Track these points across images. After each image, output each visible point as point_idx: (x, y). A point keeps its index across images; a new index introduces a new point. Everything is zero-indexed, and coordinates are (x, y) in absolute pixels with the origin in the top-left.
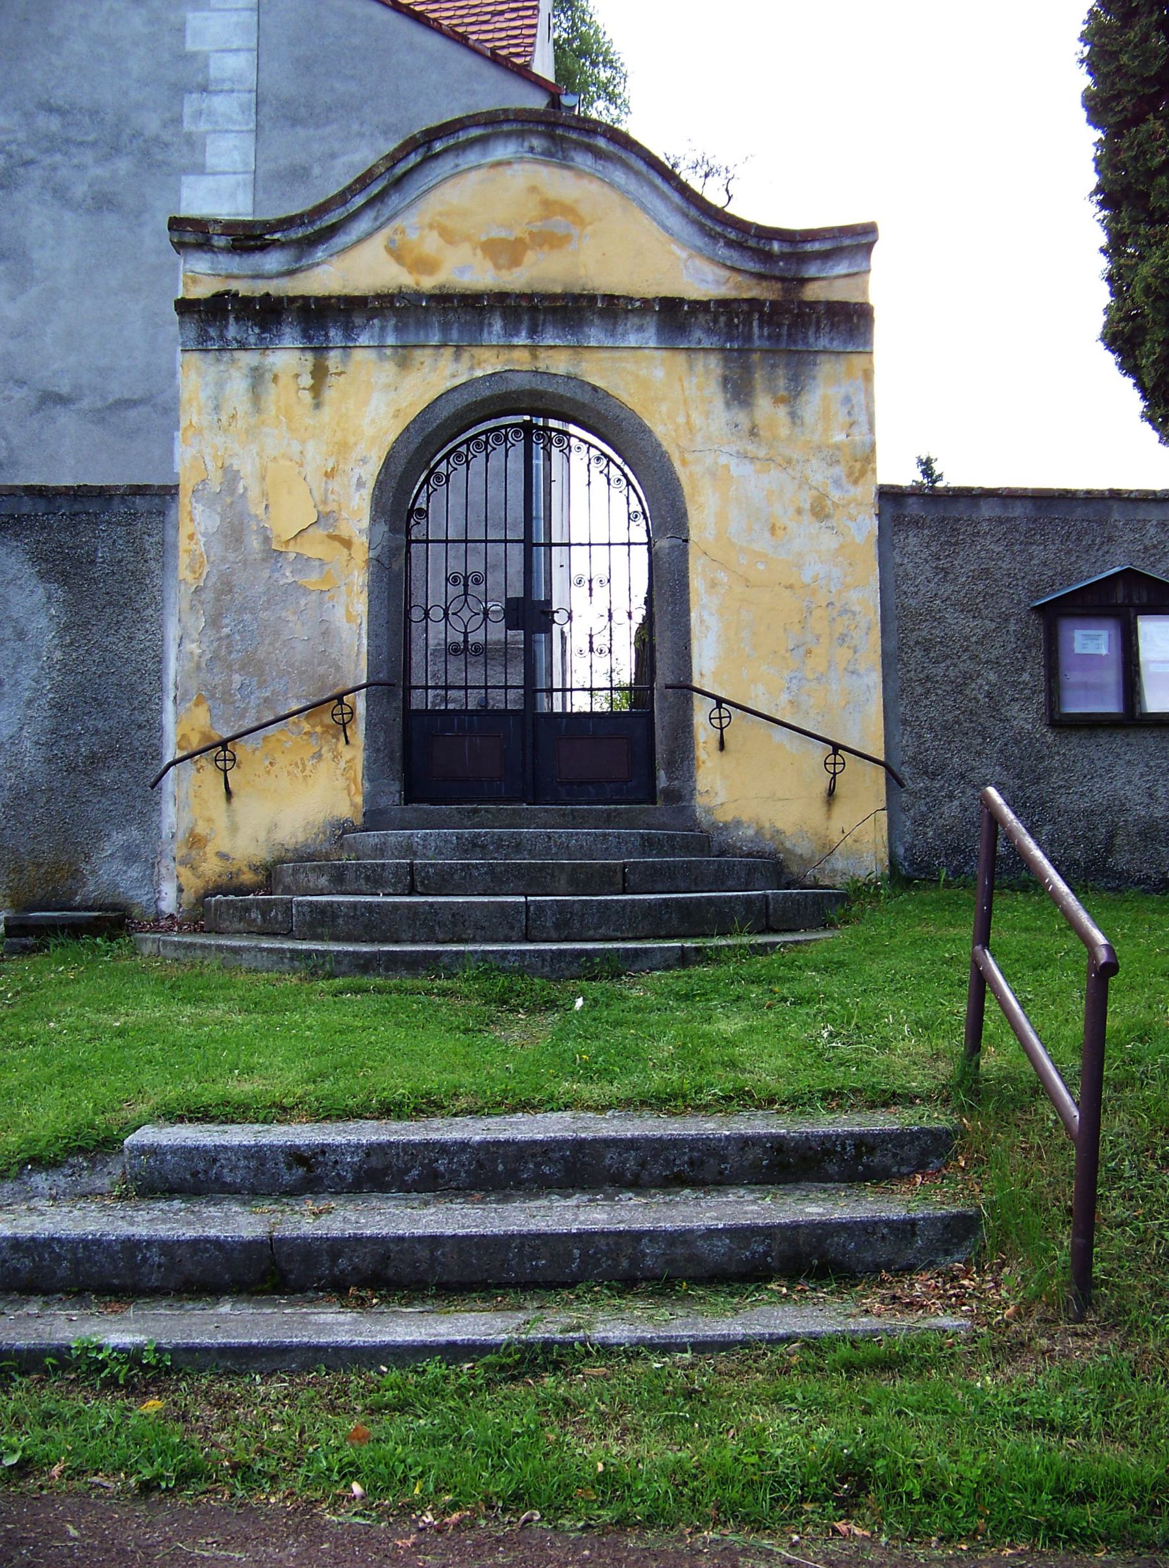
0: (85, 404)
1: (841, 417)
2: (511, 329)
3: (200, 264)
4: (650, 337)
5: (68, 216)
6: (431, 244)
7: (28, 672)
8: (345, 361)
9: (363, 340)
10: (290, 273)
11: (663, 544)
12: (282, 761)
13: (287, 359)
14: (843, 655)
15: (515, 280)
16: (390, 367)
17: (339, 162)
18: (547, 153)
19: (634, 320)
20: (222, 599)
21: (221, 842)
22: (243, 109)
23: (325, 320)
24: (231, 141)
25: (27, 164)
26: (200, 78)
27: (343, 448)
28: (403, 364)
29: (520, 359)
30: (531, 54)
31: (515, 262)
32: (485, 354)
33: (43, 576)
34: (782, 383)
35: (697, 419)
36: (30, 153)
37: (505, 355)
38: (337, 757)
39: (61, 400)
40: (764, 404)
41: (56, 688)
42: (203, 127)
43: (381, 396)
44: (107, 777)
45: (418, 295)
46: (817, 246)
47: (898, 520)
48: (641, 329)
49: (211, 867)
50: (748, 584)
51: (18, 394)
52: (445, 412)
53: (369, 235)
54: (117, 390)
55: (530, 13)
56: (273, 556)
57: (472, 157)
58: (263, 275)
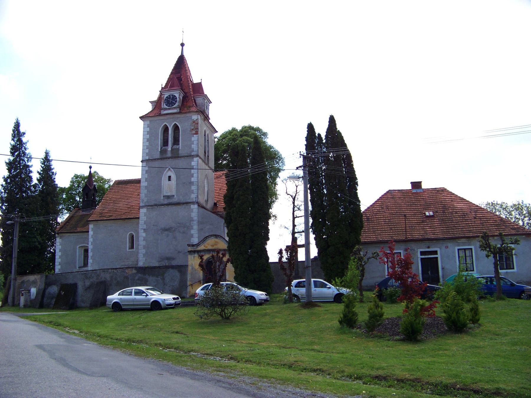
3: (190, 248)
6: (207, 245)
15: (213, 248)
56: (195, 270)
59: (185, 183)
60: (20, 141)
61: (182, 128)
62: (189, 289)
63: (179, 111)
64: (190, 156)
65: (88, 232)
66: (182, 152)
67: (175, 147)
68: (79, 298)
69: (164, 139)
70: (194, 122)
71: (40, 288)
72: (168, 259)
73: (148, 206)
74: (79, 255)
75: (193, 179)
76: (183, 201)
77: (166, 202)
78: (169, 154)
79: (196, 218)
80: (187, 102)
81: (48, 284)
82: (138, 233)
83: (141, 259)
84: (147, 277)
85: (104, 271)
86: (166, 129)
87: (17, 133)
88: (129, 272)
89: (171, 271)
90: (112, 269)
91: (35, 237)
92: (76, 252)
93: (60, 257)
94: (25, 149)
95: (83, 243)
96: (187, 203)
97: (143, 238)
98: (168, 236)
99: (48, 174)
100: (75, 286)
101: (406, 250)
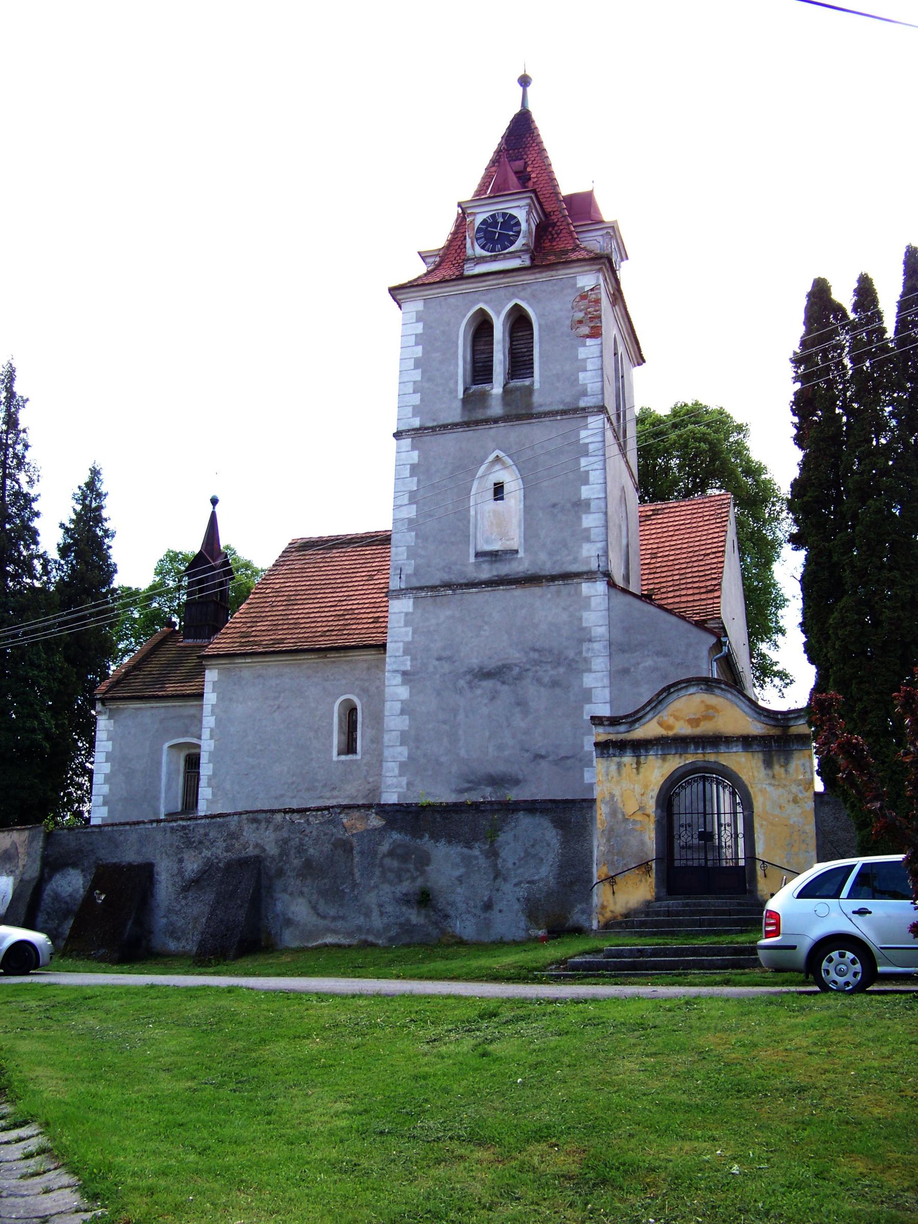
0: (550, 758)
1: (801, 769)
2: (696, 748)
3: (600, 730)
4: (740, 749)
5: (542, 689)
6: (671, 721)
7: (551, 856)
8: (646, 759)
9: (651, 753)
10: (628, 732)
11: (746, 813)
12: (630, 882)
13: (628, 759)
14: (803, 846)
16: (660, 761)
17: (641, 666)
18: (707, 690)
19: (734, 744)
20: (610, 833)
21: (611, 907)
22: (605, 647)
23: (640, 747)
24: (600, 660)
25: (528, 670)
26: (588, 636)
27: (646, 786)
28: (664, 760)
29: (700, 757)
30: (721, 578)
31: (698, 725)
32: (689, 756)
33: (555, 827)
34: (782, 760)
35: (756, 774)
36: (528, 666)
37: (695, 756)
38: (646, 881)
39: (542, 757)
40: (777, 768)
41: (559, 861)
42: (590, 654)
43: (657, 771)
44: (576, 888)
45: (667, 738)
46: (793, 716)
47: (821, 802)
48: (737, 746)
49: (608, 915)
50: (773, 824)
51: (526, 755)
52: (677, 774)
53: (652, 719)
54: (562, 753)
55: (720, 554)
56: (626, 820)
57: (683, 692)
58: (620, 733)
59: (556, 504)
61: (540, 316)
63: (527, 263)
64: (575, 412)
65: (200, 696)
66: (540, 400)
68: (160, 922)
69: (474, 361)
70: (584, 297)
71: (27, 877)
72: (495, 781)
73: (421, 588)
74: (169, 774)
75: (586, 492)
76: (549, 568)
77: (485, 575)
78: (496, 408)
79: (600, 631)
80: (551, 241)
81: (52, 864)
82: (377, 698)
83: (390, 781)
84: (426, 842)
85: (255, 821)
88: (353, 823)
89: (525, 821)
90: (285, 811)
91: (36, 717)
92: (159, 763)
93: (108, 779)
94: (26, 447)
95: (186, 733)
96: (566, 576)
97: (398, 706)
98: (494, 696)
99: (90, 530)
100: (146, 872)
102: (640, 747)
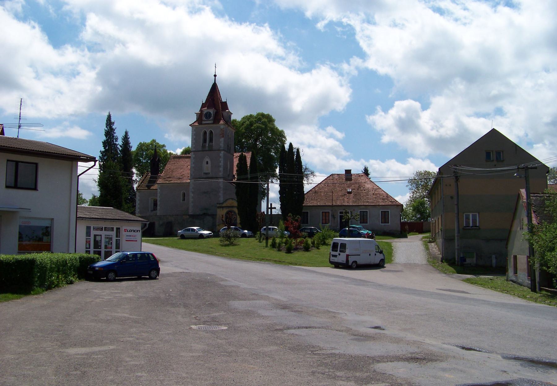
23: (223, 207)
60: (111, 127)
62: (218, 227)
64: (219, 150)
67: (211, 144)
75: (220, 164)
78: (207, 149)
86: (205, 133)
87: (109, 122)
101: (332, 211)
102: (223, 207)
